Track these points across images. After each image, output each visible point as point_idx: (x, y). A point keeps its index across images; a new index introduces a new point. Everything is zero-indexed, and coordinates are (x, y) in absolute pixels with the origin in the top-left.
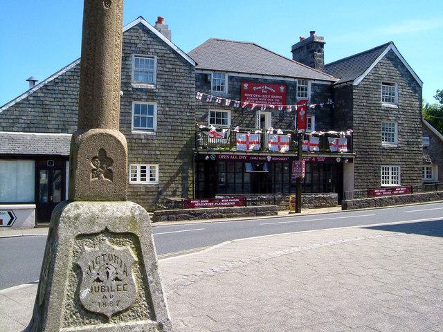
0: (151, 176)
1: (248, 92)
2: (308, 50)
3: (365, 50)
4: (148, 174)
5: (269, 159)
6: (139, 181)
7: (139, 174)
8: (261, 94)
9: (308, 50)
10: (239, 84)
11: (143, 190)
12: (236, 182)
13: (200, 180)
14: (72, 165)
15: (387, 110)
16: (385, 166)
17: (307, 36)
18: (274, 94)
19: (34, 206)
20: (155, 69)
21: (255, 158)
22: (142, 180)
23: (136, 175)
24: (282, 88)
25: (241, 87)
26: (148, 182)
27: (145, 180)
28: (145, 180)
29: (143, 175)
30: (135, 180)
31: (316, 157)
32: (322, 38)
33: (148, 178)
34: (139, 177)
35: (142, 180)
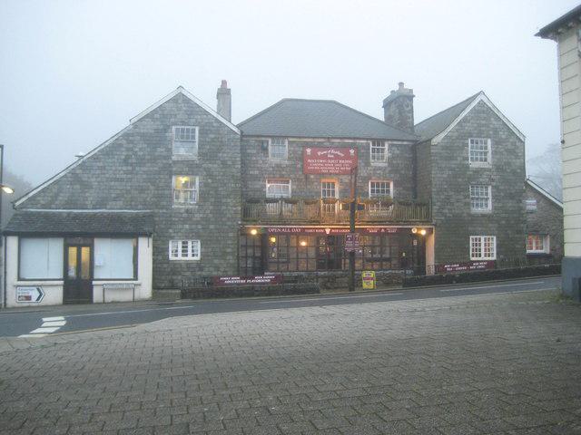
0: (193, 251)
1: (311, 158)
2: (400, 103)
3: (358, 110)
4: (190, 249)
5: (328, 231)
6: (180, 257)
7: (180, 249)
8: (327, 159)
9: (400, 103)
10: (301, 149)
11: (184, 266)
12: (300, 256)
13: (280, 266)
14: (16, 201)
15: (478, 172)
16: (474, 237)
17: (396, 88)
18: (342, 159)
19: (62, 282)
20: (197, 140)
21: (311, 231)
22: (183, 255)
23: (177, 251)
24: (352, 151)
25: (304, 153)
26: (190, 258)
27: (187, 255)
28: (187, 255)
29: (185, 251)
30: (176, 256)
31: (385, 229)
32: (411, 91)
33: (190, 253)
34: (180, 253)
35: (183, 255)
